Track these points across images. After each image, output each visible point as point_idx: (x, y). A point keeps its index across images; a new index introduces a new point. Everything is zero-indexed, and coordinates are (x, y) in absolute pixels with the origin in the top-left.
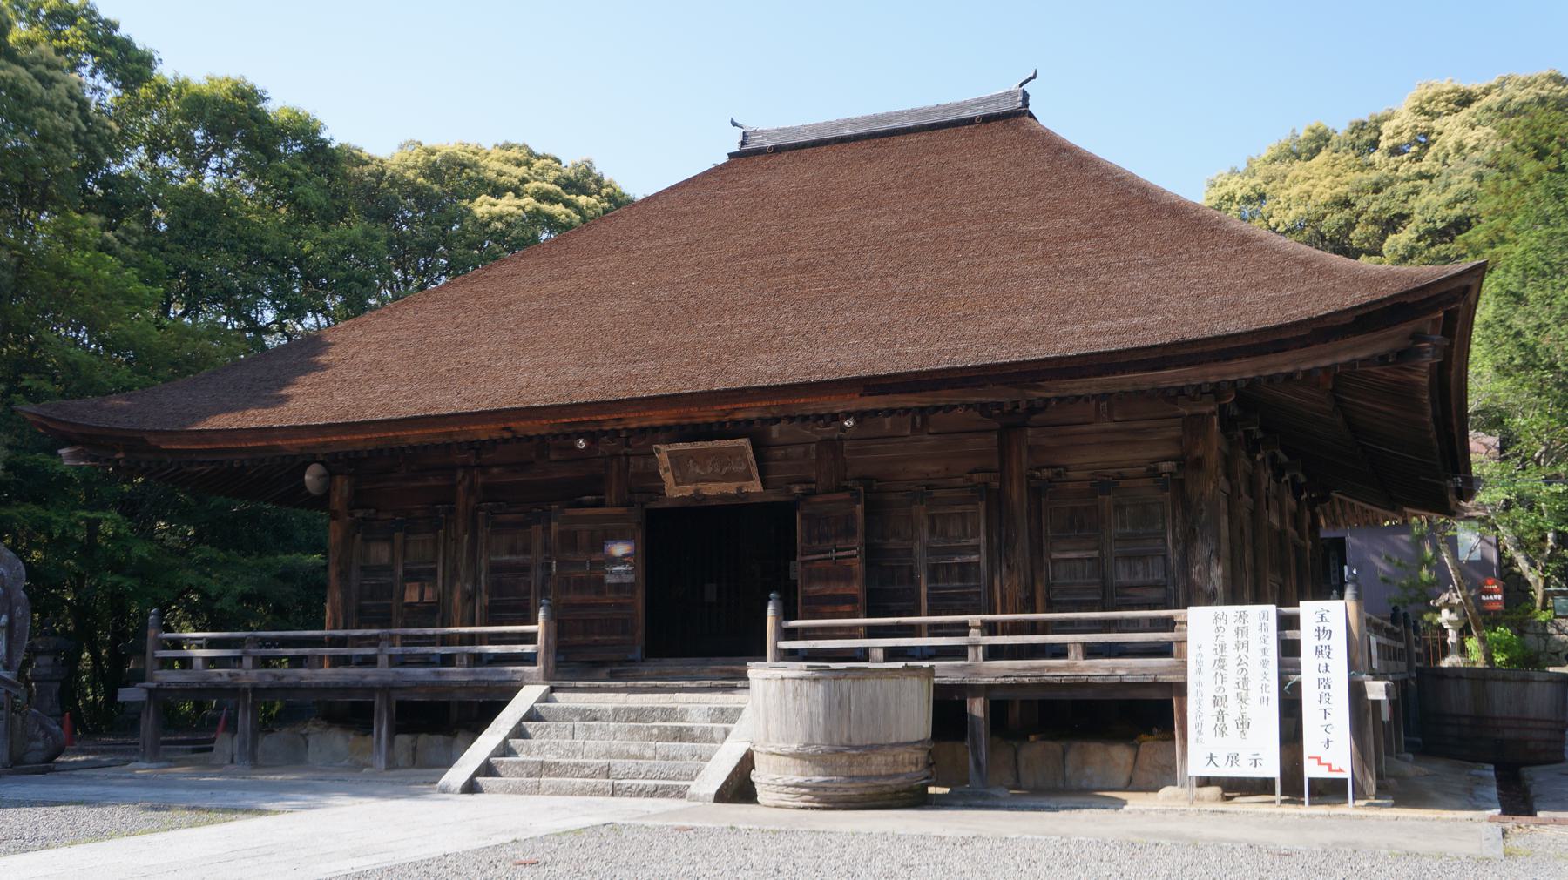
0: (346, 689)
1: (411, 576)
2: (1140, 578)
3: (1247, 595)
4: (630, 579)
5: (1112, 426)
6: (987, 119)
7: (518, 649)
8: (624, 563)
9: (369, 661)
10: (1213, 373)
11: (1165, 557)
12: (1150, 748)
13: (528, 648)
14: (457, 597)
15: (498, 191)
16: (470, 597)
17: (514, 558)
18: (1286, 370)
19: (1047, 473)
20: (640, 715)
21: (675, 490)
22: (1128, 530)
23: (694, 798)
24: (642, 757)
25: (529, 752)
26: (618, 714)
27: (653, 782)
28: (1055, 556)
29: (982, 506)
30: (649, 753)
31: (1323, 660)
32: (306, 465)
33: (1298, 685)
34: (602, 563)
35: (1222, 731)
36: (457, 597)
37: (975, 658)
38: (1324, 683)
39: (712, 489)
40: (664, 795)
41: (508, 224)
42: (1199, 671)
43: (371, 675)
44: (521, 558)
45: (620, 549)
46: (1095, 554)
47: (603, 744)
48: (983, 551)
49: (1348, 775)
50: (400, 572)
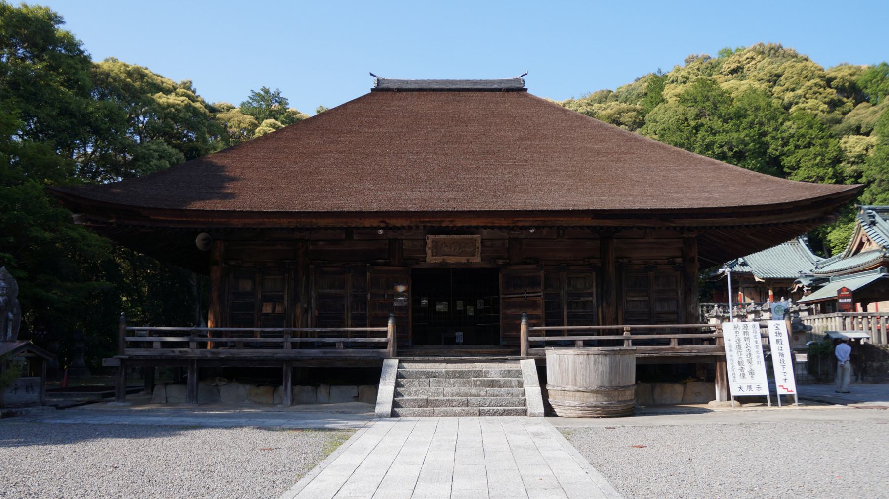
0: (265, 360)
1: (266, 299)
2: (666, 309)
3: (517, 322)
4: (404, 304)
5: (652, 240)
6: (508, 90)
7: (377, 339)
8: (403, 296)
9: (279, 346)
10: (745, 221)
11: (677, 301)
12: (365, 389)
13: (383, 340)
14: (299, 311)
15: (168, 92)
16: (306, 311)
17: (333, 291)
18: (775, 222)
19: (625, 260)
20: (461, 374)
21: (431, 259)
22: (661, 288)
23: (533, 415)
24: (479, 396)
25: (410, 394)
26: (448, 374)
27: (502, 408)
28: (628, 299)
29: (594, 274)
30: (482, 393)
31: (780, 346)
32: (196, 233)
33: (770, 356)
34: (393, 296)
35: (744, 376)
36: (299, 311)
37: (674, 344)
38: (782, 355)
39: (452, 260)
40: (508, 414)
41: (177, 110)
42: (731, 350)
43: (279, 353)
44: (338, 291)
45: (401, 289)
46: (647, 298)
47: (455, 389)
48: (594, 295)
49: (795, 392)
50: (260, 296)
